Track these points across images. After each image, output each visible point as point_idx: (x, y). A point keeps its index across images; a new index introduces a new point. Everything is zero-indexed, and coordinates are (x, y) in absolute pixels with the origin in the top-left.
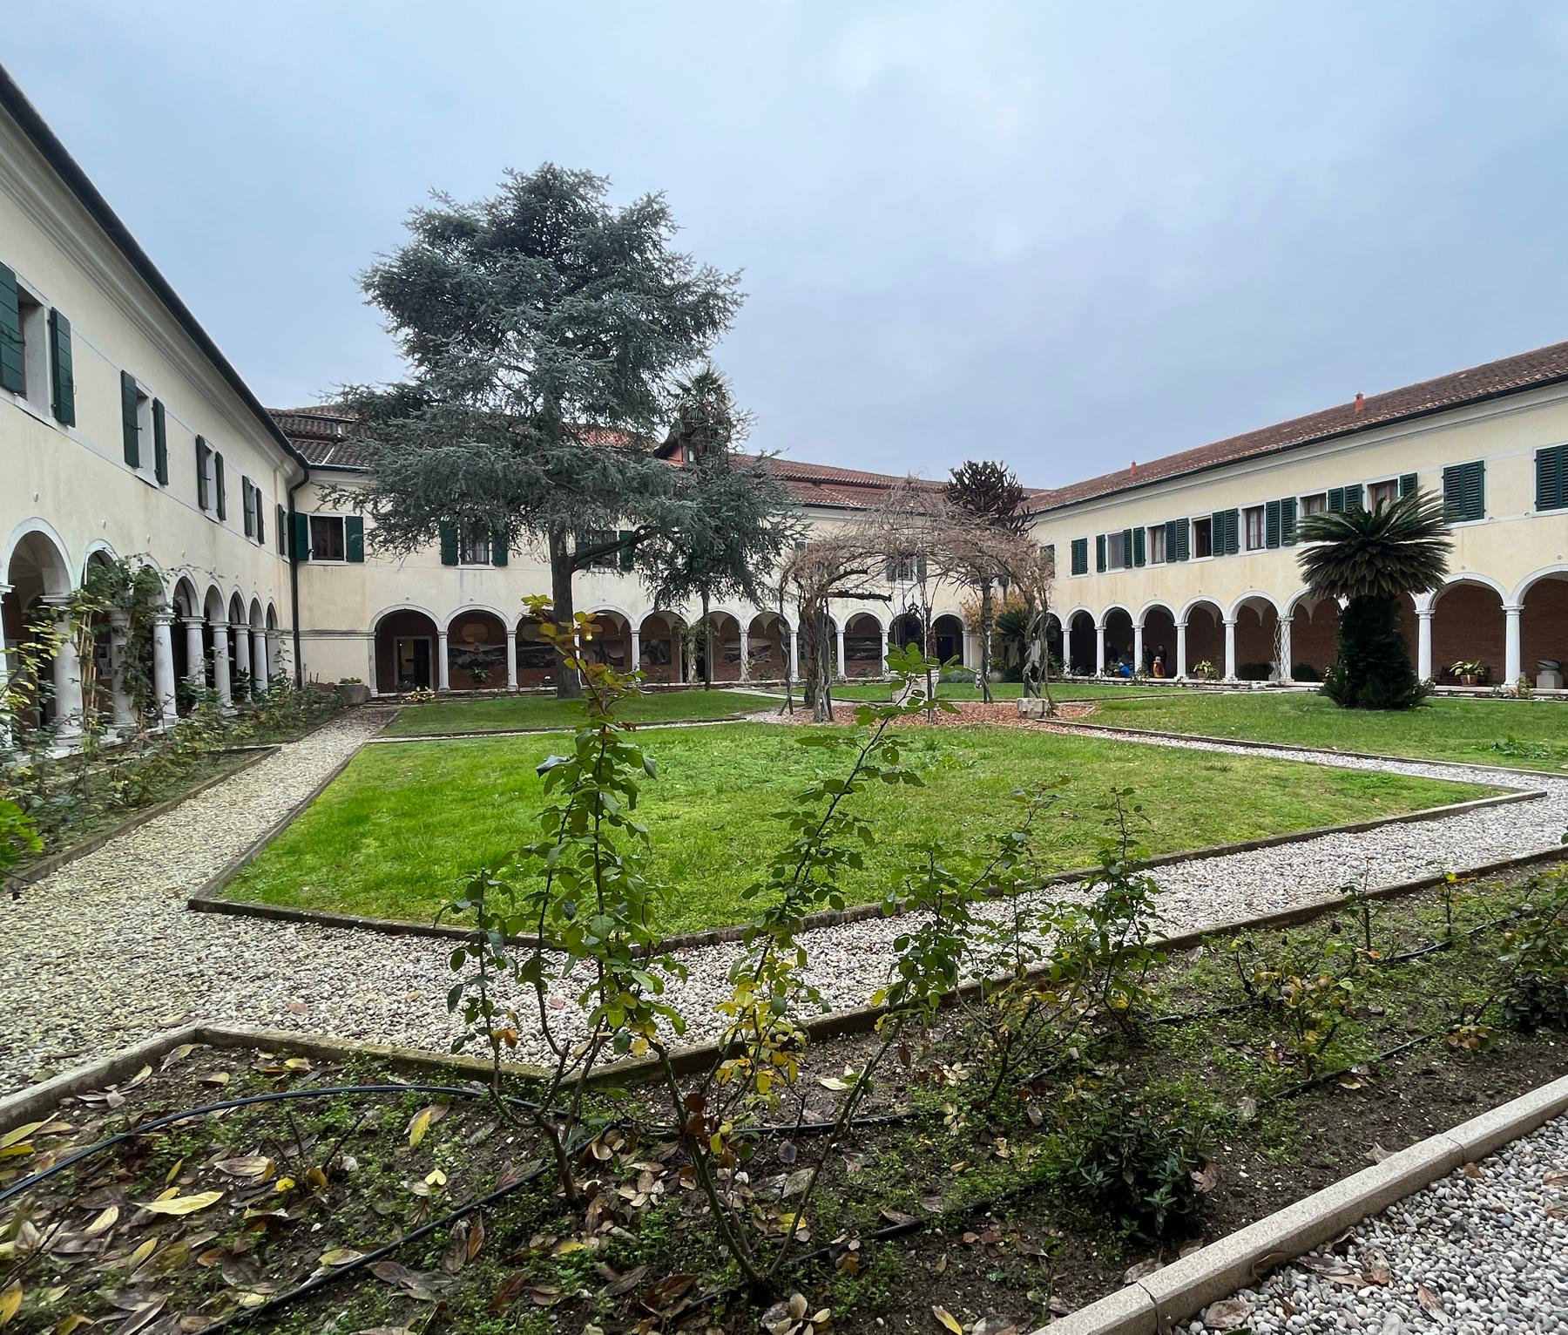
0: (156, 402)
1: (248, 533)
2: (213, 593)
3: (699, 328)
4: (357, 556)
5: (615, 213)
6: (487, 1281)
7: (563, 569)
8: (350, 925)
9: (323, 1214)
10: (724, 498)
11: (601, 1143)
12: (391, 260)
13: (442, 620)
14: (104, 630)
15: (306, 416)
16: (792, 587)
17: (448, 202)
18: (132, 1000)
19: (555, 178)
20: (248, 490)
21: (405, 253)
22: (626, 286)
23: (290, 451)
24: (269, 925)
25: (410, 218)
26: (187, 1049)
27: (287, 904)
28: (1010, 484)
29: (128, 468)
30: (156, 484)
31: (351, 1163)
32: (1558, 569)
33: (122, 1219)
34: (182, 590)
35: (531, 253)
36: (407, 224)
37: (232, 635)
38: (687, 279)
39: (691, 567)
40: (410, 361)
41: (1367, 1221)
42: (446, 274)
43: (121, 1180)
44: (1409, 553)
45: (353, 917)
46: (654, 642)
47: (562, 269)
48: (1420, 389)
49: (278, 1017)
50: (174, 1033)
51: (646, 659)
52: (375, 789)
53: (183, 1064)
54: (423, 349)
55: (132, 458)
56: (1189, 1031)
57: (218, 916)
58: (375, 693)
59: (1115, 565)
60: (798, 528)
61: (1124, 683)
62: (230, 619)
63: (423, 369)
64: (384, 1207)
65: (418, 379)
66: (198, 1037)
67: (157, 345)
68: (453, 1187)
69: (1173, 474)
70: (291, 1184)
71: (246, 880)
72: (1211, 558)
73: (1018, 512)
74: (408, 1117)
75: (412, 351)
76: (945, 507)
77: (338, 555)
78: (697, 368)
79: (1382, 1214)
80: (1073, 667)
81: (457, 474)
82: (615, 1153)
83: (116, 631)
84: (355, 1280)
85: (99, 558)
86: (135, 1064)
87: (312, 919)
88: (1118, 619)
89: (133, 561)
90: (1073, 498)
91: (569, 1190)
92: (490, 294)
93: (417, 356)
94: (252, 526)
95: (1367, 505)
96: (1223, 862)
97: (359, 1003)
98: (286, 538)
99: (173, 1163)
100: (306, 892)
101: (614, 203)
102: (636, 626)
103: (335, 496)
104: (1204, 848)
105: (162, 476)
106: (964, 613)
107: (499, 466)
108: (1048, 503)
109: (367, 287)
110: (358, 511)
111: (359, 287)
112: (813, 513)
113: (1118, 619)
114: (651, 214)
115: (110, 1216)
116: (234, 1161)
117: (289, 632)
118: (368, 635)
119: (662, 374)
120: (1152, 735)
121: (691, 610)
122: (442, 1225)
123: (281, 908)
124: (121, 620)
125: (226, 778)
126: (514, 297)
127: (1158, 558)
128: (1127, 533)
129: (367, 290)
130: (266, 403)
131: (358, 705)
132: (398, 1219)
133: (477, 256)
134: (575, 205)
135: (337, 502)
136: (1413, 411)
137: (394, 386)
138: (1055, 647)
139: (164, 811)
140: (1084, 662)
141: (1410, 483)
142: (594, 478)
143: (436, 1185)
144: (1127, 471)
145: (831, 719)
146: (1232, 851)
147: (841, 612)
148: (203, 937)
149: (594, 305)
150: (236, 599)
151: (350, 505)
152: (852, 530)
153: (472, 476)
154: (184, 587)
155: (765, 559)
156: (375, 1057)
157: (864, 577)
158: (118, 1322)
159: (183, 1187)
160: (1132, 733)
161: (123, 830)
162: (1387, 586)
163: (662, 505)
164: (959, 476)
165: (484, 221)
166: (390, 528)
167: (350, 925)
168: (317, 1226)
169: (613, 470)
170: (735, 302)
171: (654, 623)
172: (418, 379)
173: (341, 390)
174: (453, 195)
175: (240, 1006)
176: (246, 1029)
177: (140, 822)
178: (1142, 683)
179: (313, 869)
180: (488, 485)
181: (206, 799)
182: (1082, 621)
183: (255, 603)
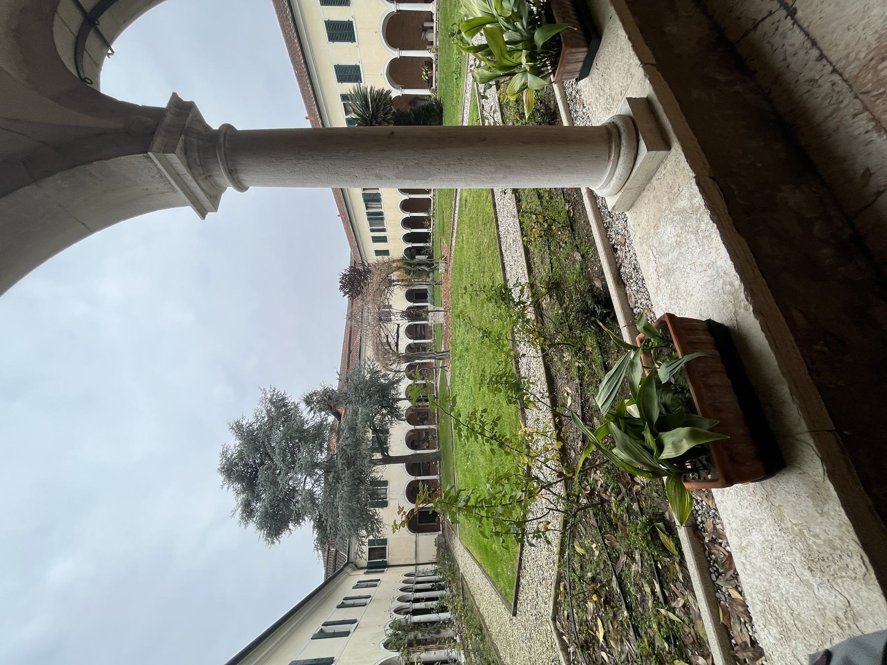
0: (323, 625)
1: (376, 586)
2: (400, 599)
3: (285, 406)
4: (385, 542)
5: (238, 442)
6: (621, 537)
7: (388, 460)
8: (521, 560)
9: (603, 586)
10: (357, 395)
11: (585, 489)
12: (262, 533)
13: (409, 506)
14: (415, 642)
15: (327, 563)
16: (394, 367)
17: (236, 511)
18: (544, 640)
19: (224, 468)
20: (359, 586)
21: (258, 528)
22: (268, 437)
23: (342, 570)
24: (521, 588)
25: (243, 526)
26: (558, 623)
27: (514, 581)
28: (349, 271)
29: (350, 635)
30: (356, 624)
31: (589, 575)
32: (381, 33)
33: (605, 651)
34: (399, 612)
35: (256, 476)
36: (246, 527)
37: (417, 600)
38: (265, 411)
39: (386, 407)
40: (302, 524)
41: (608, 236)
42: (267, 512)
43: (594, 650)
44: (375, 106)
45: (518, 558)
46: (418, 419)
47: (262, 464)
48: (303, 91)
49: (549, 590)
50: (552, 627)
51: (425, 422)
52: (475, 540)
53: (562, 625)
54: (298, 518)
55: (347, 634)
56: (556, 264)
57: (518, 606)
58: (441, 533)
59: (383, 225)
60: (369, 363)
61: (433, 221)
62: (410, 592)
63: (306, 518)
64: (602, 566)
65: (310, 520)
66: (554, 619)
67: (301, 624)
68: (597, 542)
69: (343, 199)
70: (595, 595)
71: (506, 595)
72: (387, 546)
73: (361, 268)
74: (577, 553)
75: (299, 524)
76: (359, 302)
77: (384, 549)
78: (302, 406)
79: (607, 229)
80: (427, 242)
81: (350, 506)
82: (588, 484)
83: (415, 637)
84: (621, 579)
85: (386, 645)
86: (562, 642)
87: (519, 573)
88: (407, 223)
89: (388, 632)
90: (354, 243)
91: (598, 504)
92: (274, 493)
93: (301, 521)
94: (373, 584)
95: (354, 116)
96: (500, 219)
97: (545, 561)
98: (378, 570)
99: (589, 633)
100: (509, 573)
101: (233, 443)
102: (412, 427)
103: (360, 553)
104: (494, 224)
105: (353, 622)
106: (404, 289)
107: (346, 489)
108: (357, 253)
109: (273, 543)
110: (366, 544)
111: (273, 546)
112: (362, 357)
113: (407, 223)
114: (238, 428)
115: (604, 654)
116: (589, 613)
117: (416, 567)
118: (416, 536)
119: (305, 420)
120: (454, 220)
121: (404, 405)
122: (606, 548)
123: (515, 584)
124: (411, 636)
125: (472, 596)
126: (275, 483)
127: (380, 206)
128: (369, 219)
129: (274, 543)
130: (322, 581)
131: (445, 540)
132: (605, 562)
133: (258, 498)
134: (235, 459)
135: (362, 552)
136: (312, 96)
137: (314, 530)
138: (419, 251)
139: (483, 620)
140: (425, 237)
141: (344, 97)
142: (350, 450)
143: (596, 547)
144: (342, 218)
145: (449, 351)
146: (495, 210)
147: (405, 342)
148: (525, 612)
149: (277, 451)
150: (403, 590)
151: (363, 547)
152: (370, 343)
153: (350, 499)
154: (398, 611)
155: (383, 376)
156: (560, 561)
157: (390, 336)
158: (631, 655)
159: (596, 630)
160: (453, 229)
161: (490, 636)
162: (389, 116)
163: (361, 422)
164: (346, 293)
165: (243, 496)
166: (373, 530)
167: (521, 560)
168: (607, 588)
169: (347, 442)
170: (274, 390)
171: (411, 420)
172: (310, 520)
173: (316, 551)
174: (233, 508)
175: (546, 603)
176: (551, 604)
177: (487, 630)
178: (433, 213)
179: (503, 569)
180: (354, 492)
181: (480, 604)
182: (408, 238)
183: (404, 582)
